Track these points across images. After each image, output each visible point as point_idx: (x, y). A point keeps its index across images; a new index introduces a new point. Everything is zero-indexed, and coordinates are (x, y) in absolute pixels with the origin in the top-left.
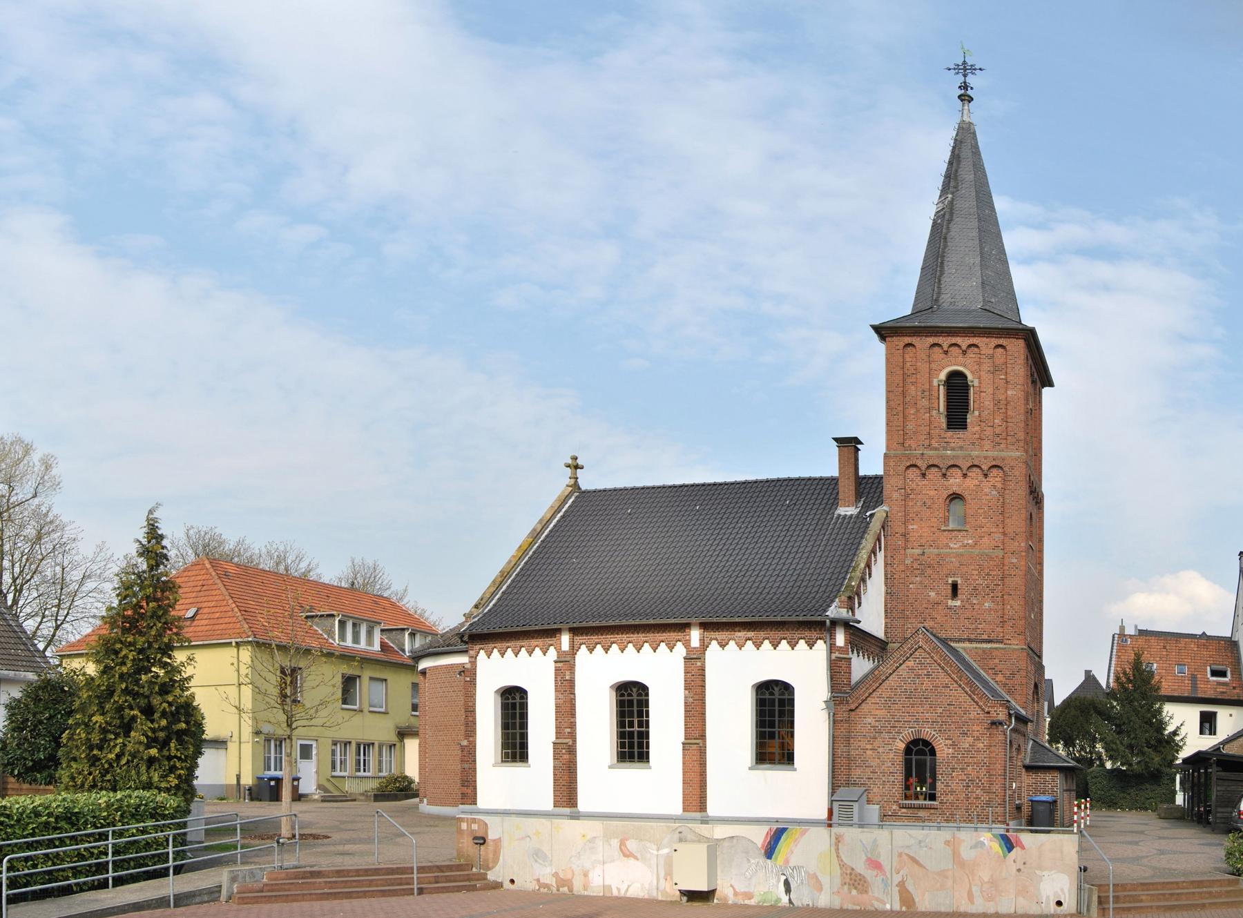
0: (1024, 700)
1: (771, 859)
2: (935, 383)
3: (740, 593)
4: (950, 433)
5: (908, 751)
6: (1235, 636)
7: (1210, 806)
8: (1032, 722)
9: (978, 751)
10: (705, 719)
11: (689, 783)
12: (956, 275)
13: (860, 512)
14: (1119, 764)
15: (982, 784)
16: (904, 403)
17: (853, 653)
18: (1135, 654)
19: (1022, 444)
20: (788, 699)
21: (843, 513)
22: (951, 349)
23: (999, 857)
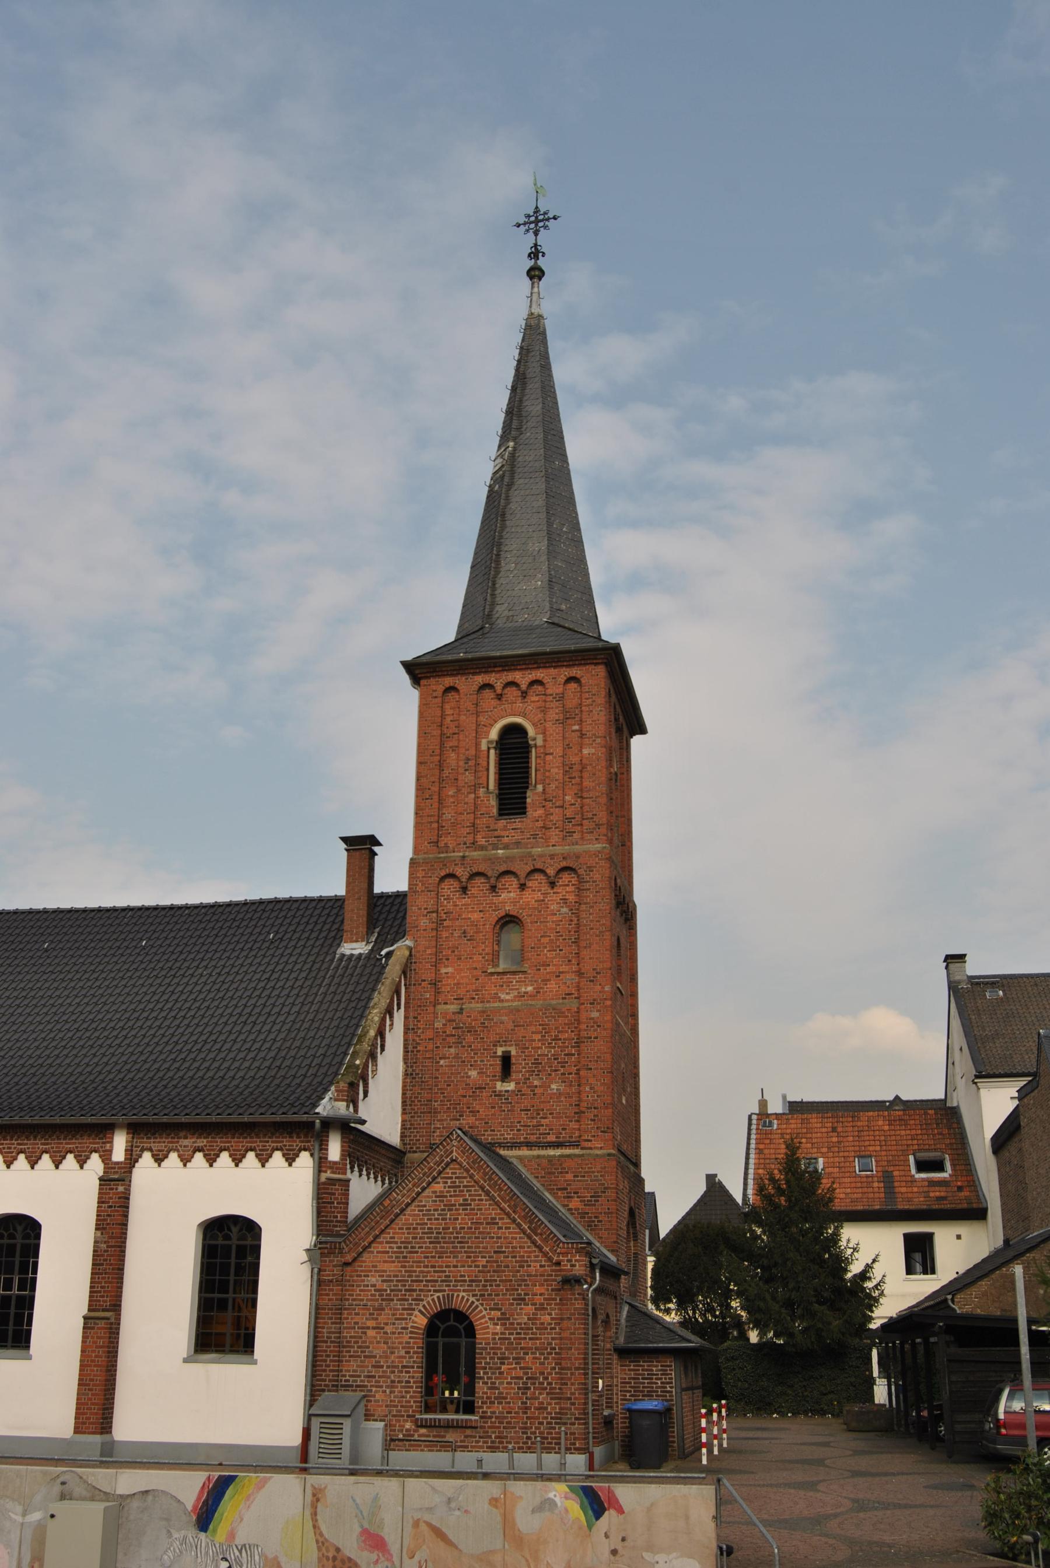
0: (614, 1238)
1: (206, 1531)
2: (484, 746)
3: (192, 1078)
4: (502, 823)
5: (431, 1329)
6: (952, 1099)
7: (940, 1407)
8: (627, 1274)
9: (542, 1328)
10: (122, 1278)
11: (88, 1385)
12: (516, 572)
13: (372, 950)
14: (771, 1334)
15: (549, 1384)
16: (441, 780)
17: (352, 1172)
18: (787, 1147)
19: (603, 830)
20: (251, 1246)
21: (348, 952)
22: (506, 691)
23: (580, 1528)
